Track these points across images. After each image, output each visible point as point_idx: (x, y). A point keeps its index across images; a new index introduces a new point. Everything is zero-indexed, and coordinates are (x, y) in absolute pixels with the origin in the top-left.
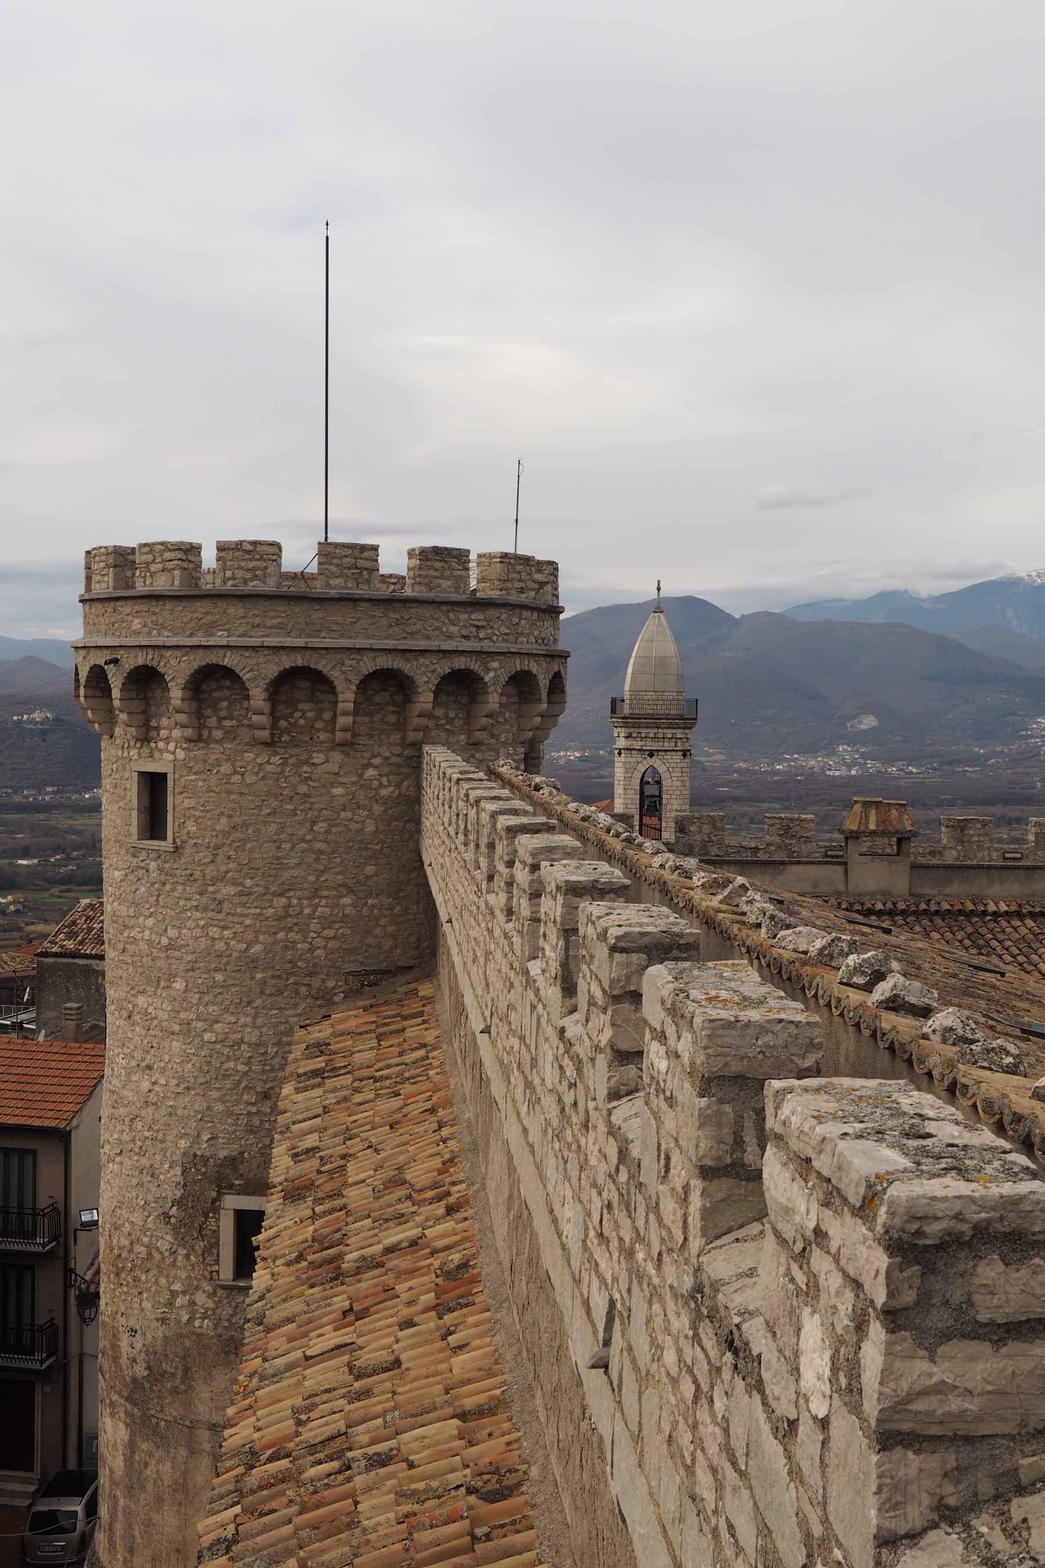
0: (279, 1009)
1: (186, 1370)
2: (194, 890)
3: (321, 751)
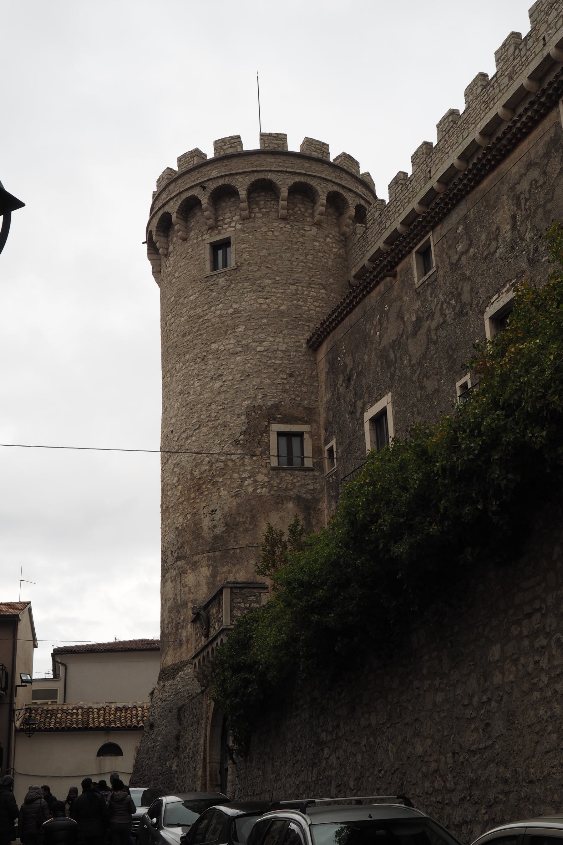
0: (295, 335)
1: (253, 517)
2: (248, 284)
3: (308, 225)
